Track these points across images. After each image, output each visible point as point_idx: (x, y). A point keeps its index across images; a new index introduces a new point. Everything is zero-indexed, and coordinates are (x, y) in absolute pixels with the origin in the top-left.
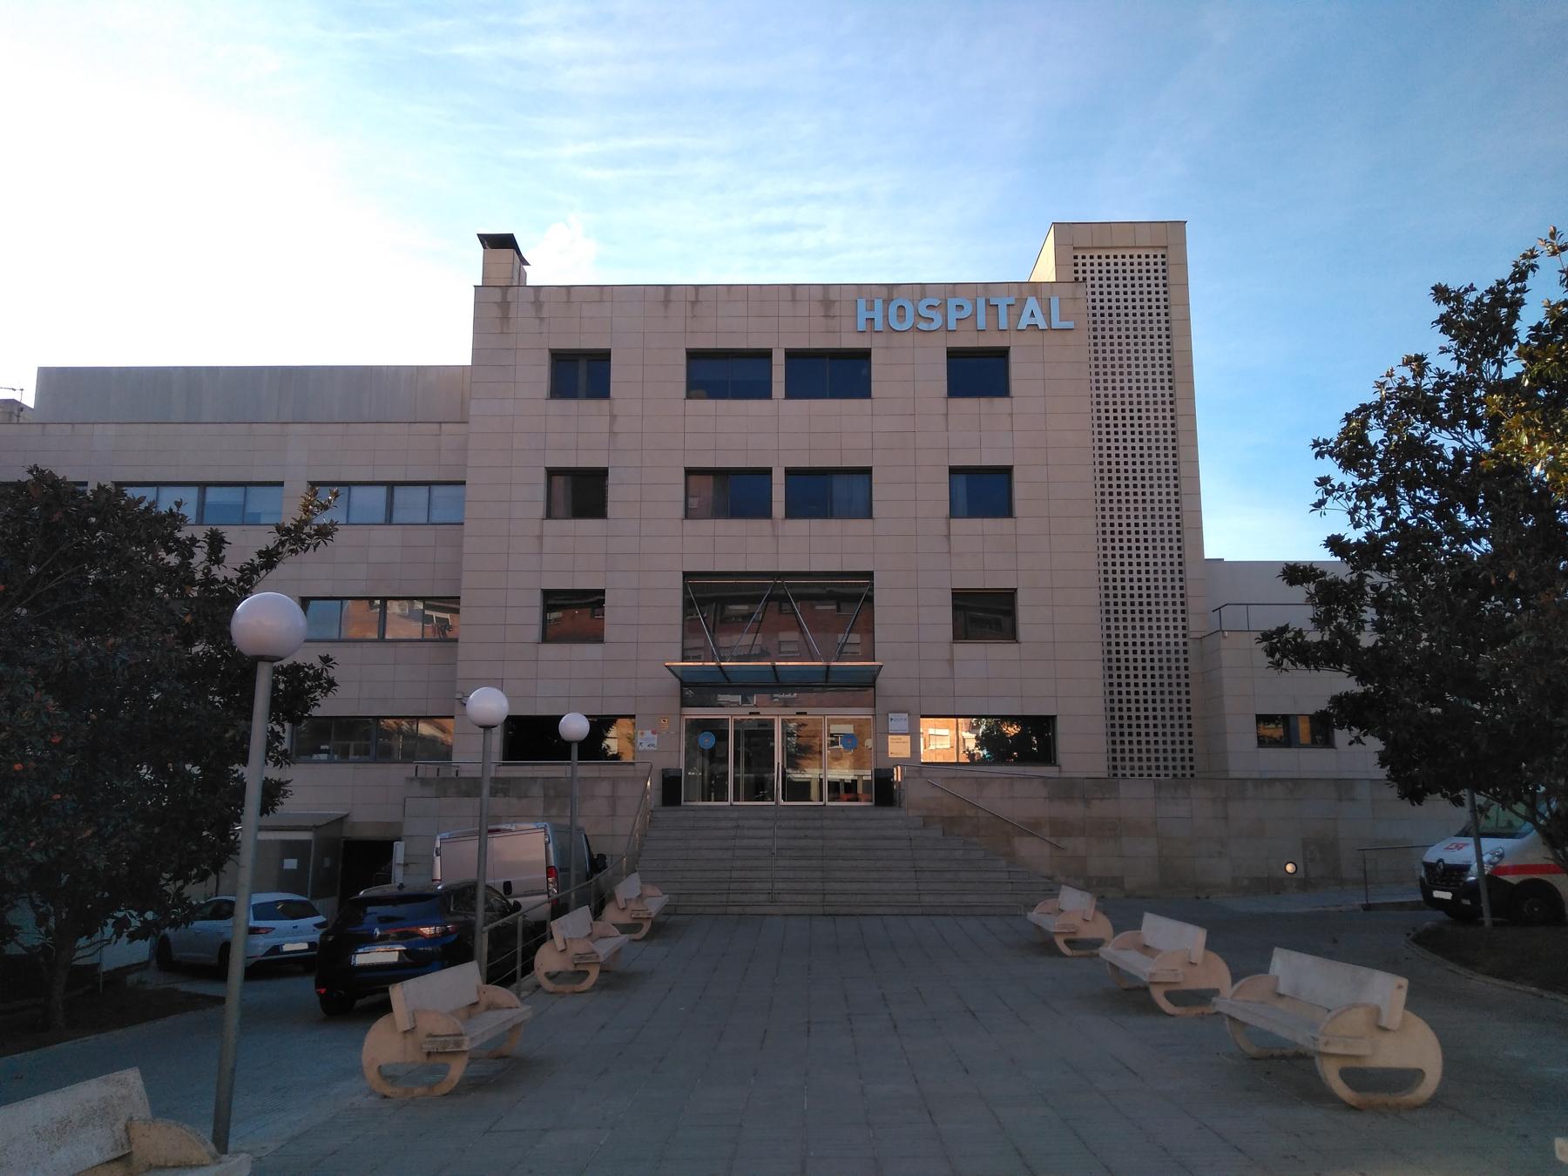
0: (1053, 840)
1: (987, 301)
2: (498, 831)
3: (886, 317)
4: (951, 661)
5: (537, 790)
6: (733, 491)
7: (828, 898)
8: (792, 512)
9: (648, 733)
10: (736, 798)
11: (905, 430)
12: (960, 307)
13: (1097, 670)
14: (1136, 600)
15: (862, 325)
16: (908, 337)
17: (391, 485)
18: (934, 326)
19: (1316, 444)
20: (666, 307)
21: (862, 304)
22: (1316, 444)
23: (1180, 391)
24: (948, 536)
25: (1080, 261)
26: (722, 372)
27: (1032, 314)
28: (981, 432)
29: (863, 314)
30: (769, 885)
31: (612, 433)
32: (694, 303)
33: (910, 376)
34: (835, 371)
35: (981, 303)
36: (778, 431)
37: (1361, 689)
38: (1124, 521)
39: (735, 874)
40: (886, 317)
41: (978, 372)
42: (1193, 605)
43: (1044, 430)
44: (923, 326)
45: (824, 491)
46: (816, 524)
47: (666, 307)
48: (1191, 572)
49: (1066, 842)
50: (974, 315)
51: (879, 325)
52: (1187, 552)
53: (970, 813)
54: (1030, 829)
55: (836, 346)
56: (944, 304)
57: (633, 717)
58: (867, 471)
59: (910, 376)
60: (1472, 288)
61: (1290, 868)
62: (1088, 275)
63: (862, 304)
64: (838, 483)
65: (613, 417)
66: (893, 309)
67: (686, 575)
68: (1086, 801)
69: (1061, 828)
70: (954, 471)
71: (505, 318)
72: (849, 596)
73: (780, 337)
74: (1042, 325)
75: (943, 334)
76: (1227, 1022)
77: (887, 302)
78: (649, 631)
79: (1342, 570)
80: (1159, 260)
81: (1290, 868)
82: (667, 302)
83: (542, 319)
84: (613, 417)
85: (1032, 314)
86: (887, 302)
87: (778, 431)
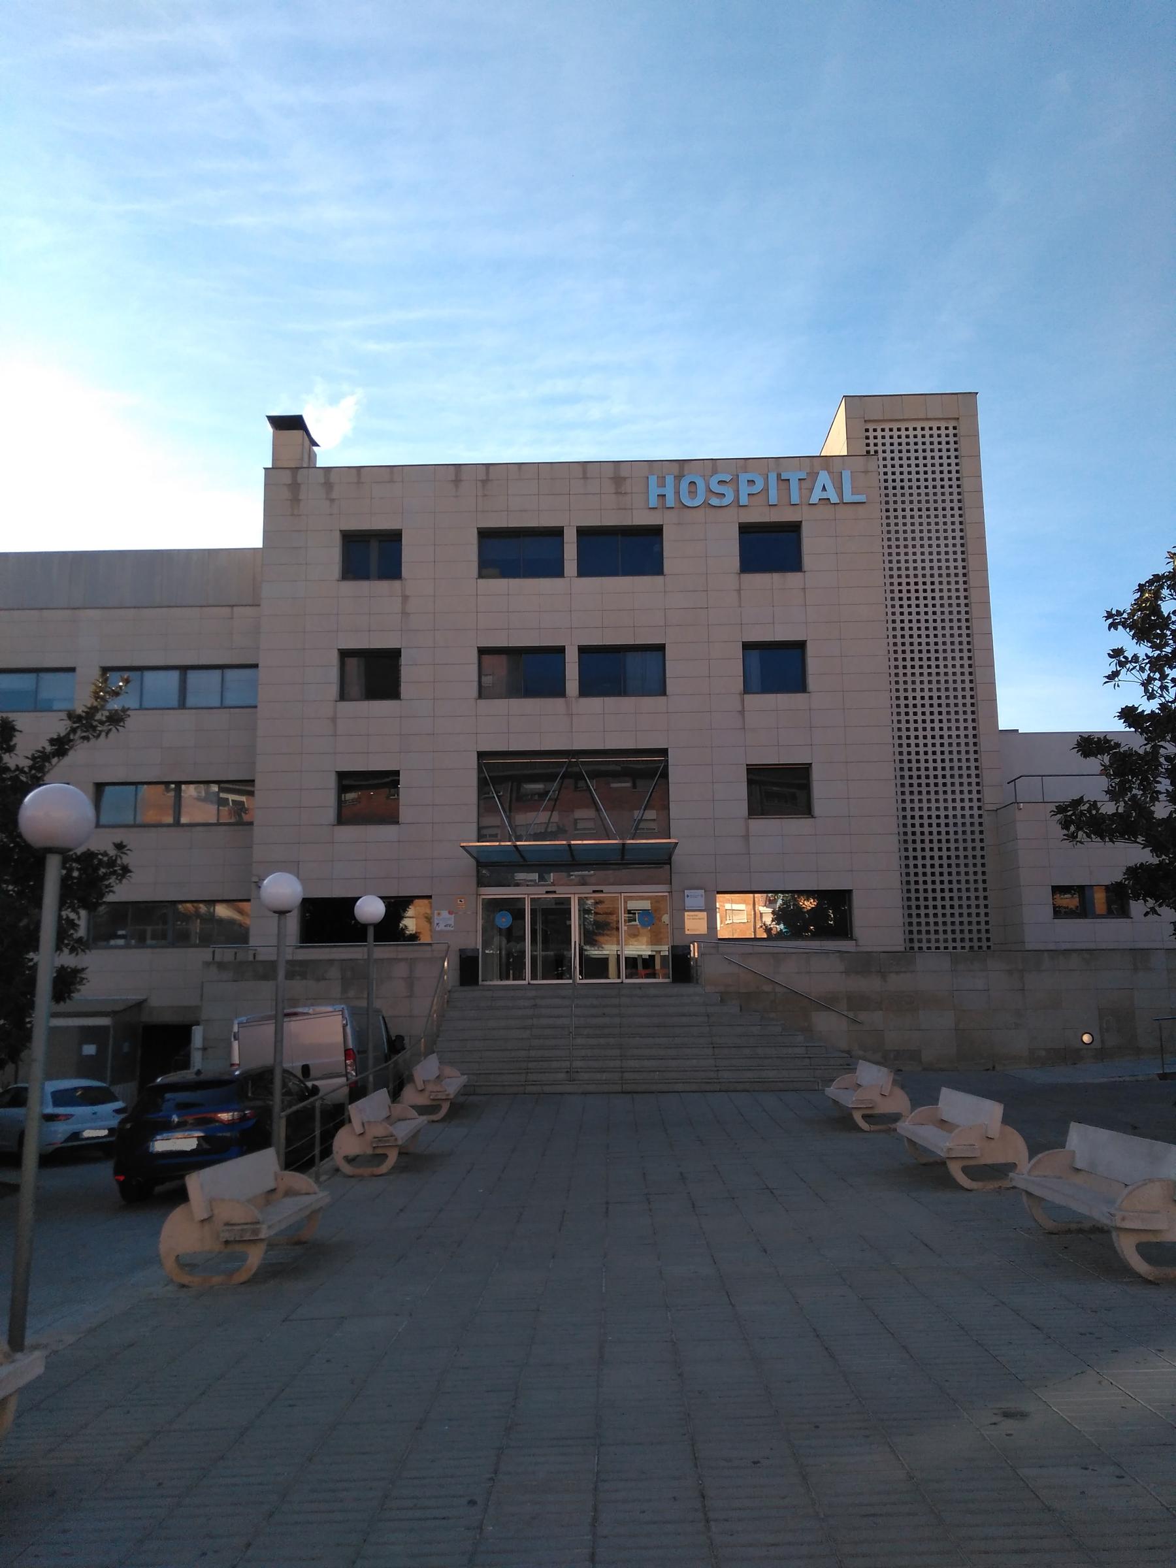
0: (851, 1014)
1: (779, 476)
2: (295, 1014)
3: (677, 493)
4: (746, 837)
6: (527, 670)
8: (586, 690)
9: (445, 913)
10: (534, 977)
11: (698, 606)
12: (751, 482)
13: (892, 843)
14: (931, 773)
15: (653, 501)
17: (184, 669)
18: (725, 502)
19: (1109, 615)
21: (653, 480)
22: (1109, 615)
23: (972, 563)
24: (742, 712)
25: (871, 434)
26: (515, 551)
27: (824, 489)
28: (774, 607)
32: (485, 482)
33: (702, 553)
35: (773, 477)
36: (572, 609)
38: (918, 694)
39: (533, 1053)
40: (677, 493)
41: (771, 546)
42: (988, 777)
43: (834, 602)
44: (714, 501)
45: (619, 669)
46: (611, 702)
48: (985, 744)
49: (863, 1016)
50: (766, 489)
51: (670, 501)
52: (982, 729)
53: (767, 988)
54: (826, 1004)
56: (735, 480)
59: (702, 553)
62: (880, 448)
63: (653, 480)
65: (405, 598)
66: (684, 485)
67: (481, 755)
69: (858, 1002)
70: (747, 646)
71: (295, 500)
72: (646, 772)
73: (571, 516)
74: (834, 499)
76: (1024, 1198)
77: (679, 478)
79: (1137, 743)
80: (951, 431)
82: (457, 481)
83: (332, 500)
84: (405, 598)
85: (824, 489)
86: (679, 478)
87: (572, 609)
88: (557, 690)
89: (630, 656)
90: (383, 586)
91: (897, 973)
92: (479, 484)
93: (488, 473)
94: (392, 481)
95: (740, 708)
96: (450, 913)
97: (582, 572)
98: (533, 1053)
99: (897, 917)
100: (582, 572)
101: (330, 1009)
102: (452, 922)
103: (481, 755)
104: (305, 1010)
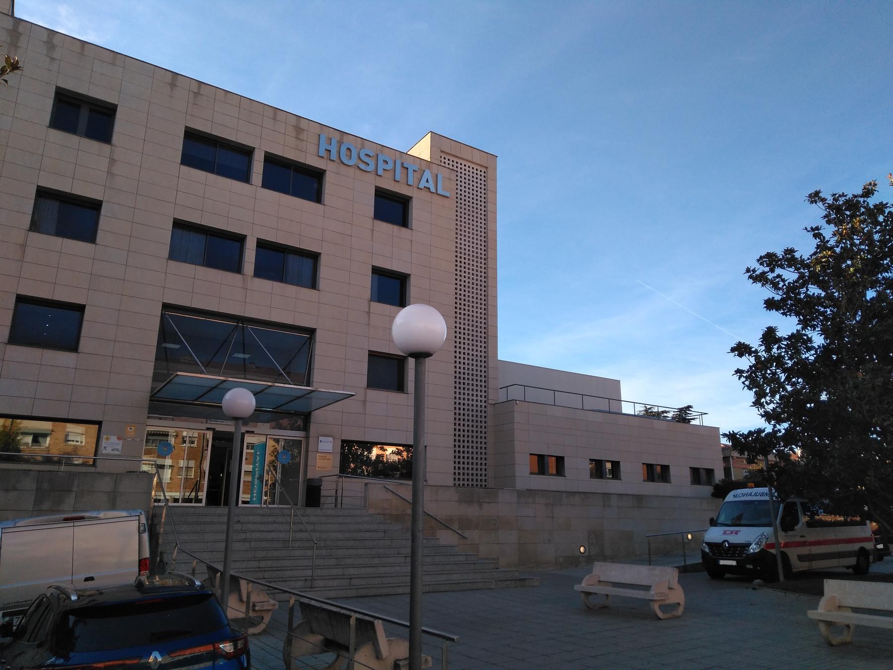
0: (459, 532)
2: (82, 518)
5: (29, 484)
6: (213, 246)
7: (354, 582)
8: (261, 272)
9: (114, 439)
12: (386, 162)
15: (322, 153)
16: (351, 171)
18: (369, 169)
20: (172, 89)
24: (369, 313)
26: (210, 152)
27: (427, 181)
29: (324, 146)
30: (309, 573)
31: (109, 172)
32: (197, 94)
33: (350, 194)
34: (298, 178)
37: (769, 429)
39: (263, 564)
41: (393, 207)
42: (491, 383)
44: (362, 166)
45: (286, 262)
46: (277, 285)
47: (172, 89)
49: (467, 534)
51: (334, 156)
54: (445, 525)
55: (302, 160)
57: (99, 423)
58: (81, 308)
59: (350, 194)
60: (843, 195)
61: (582, 549)
64: (292, 259)
65: (113, 161)
67: (166, 306)
68: (480, 504)
69: (466, 523)
73: (264, 143)
74: (433, 190)
75: (373, 176)
78: (121, 350)
80: (482, 173)
81: (582, 549)
83: (53, 59)
85: (427, 181)
86: (340, 143)
88: (236, 267)
89: (291, 258)
90: (93, 146)
91: (488, 503)
92: (191, 94)
93: (199, 88)
94: (113, 64)
95: (367, 310)
96: (119, 438)
97: (266, 184)
98: (263, 564)
99: (449, 467)
100: (266, 184)
101: (124, 514)
102: (120, 447)
103: (166, 306)
104: (94, 514)
